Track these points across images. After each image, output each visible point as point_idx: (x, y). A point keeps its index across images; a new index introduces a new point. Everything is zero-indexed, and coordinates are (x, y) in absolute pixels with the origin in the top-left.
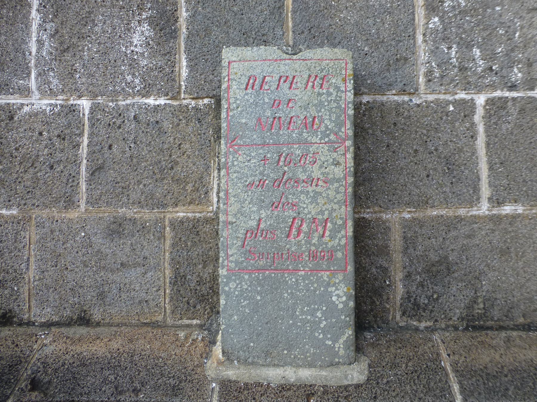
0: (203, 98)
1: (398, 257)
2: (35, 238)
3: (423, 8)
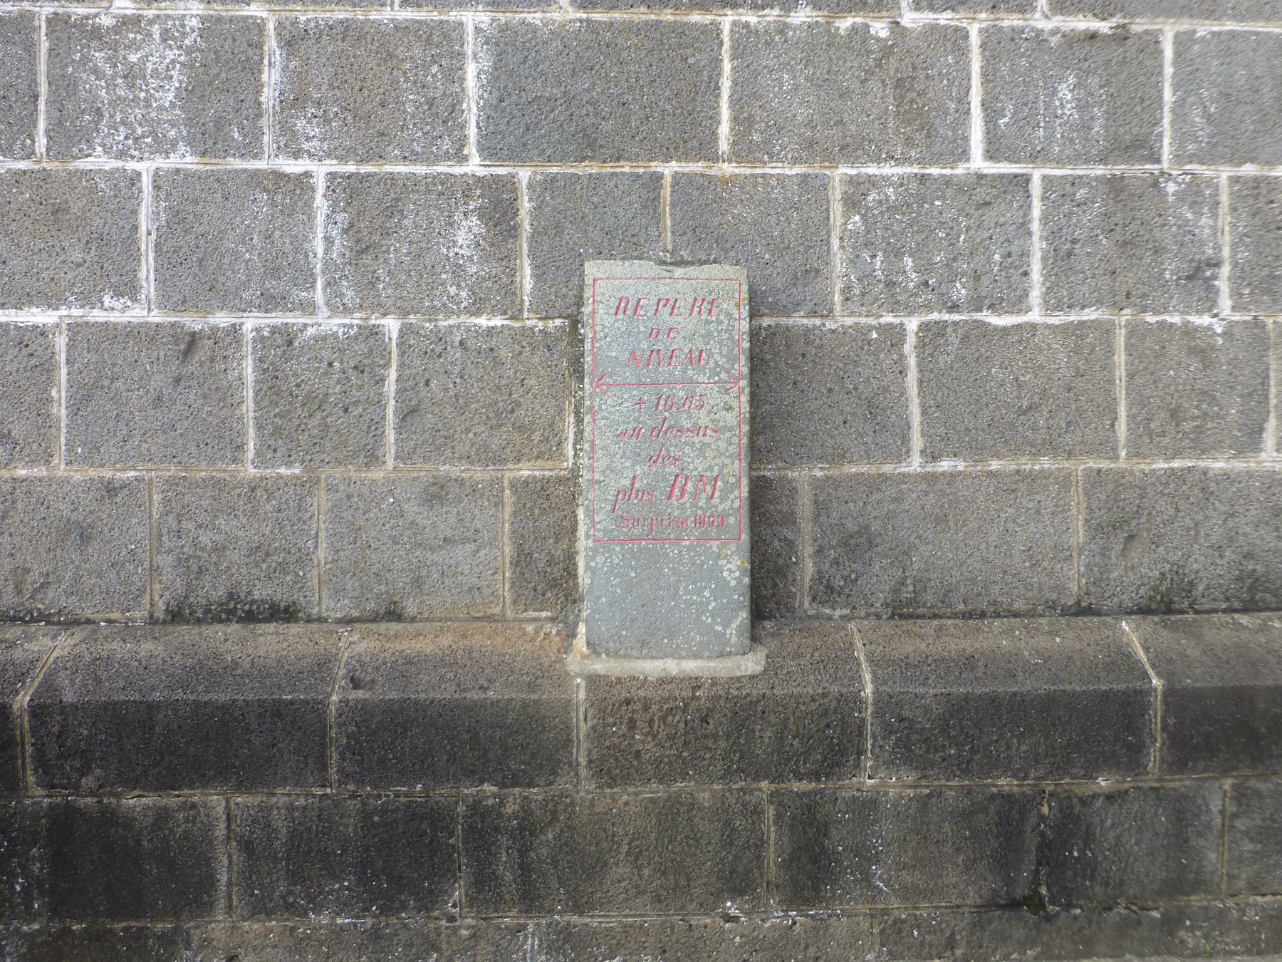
0: (553, 318)
1: (807, 527)
2: (325, 505)
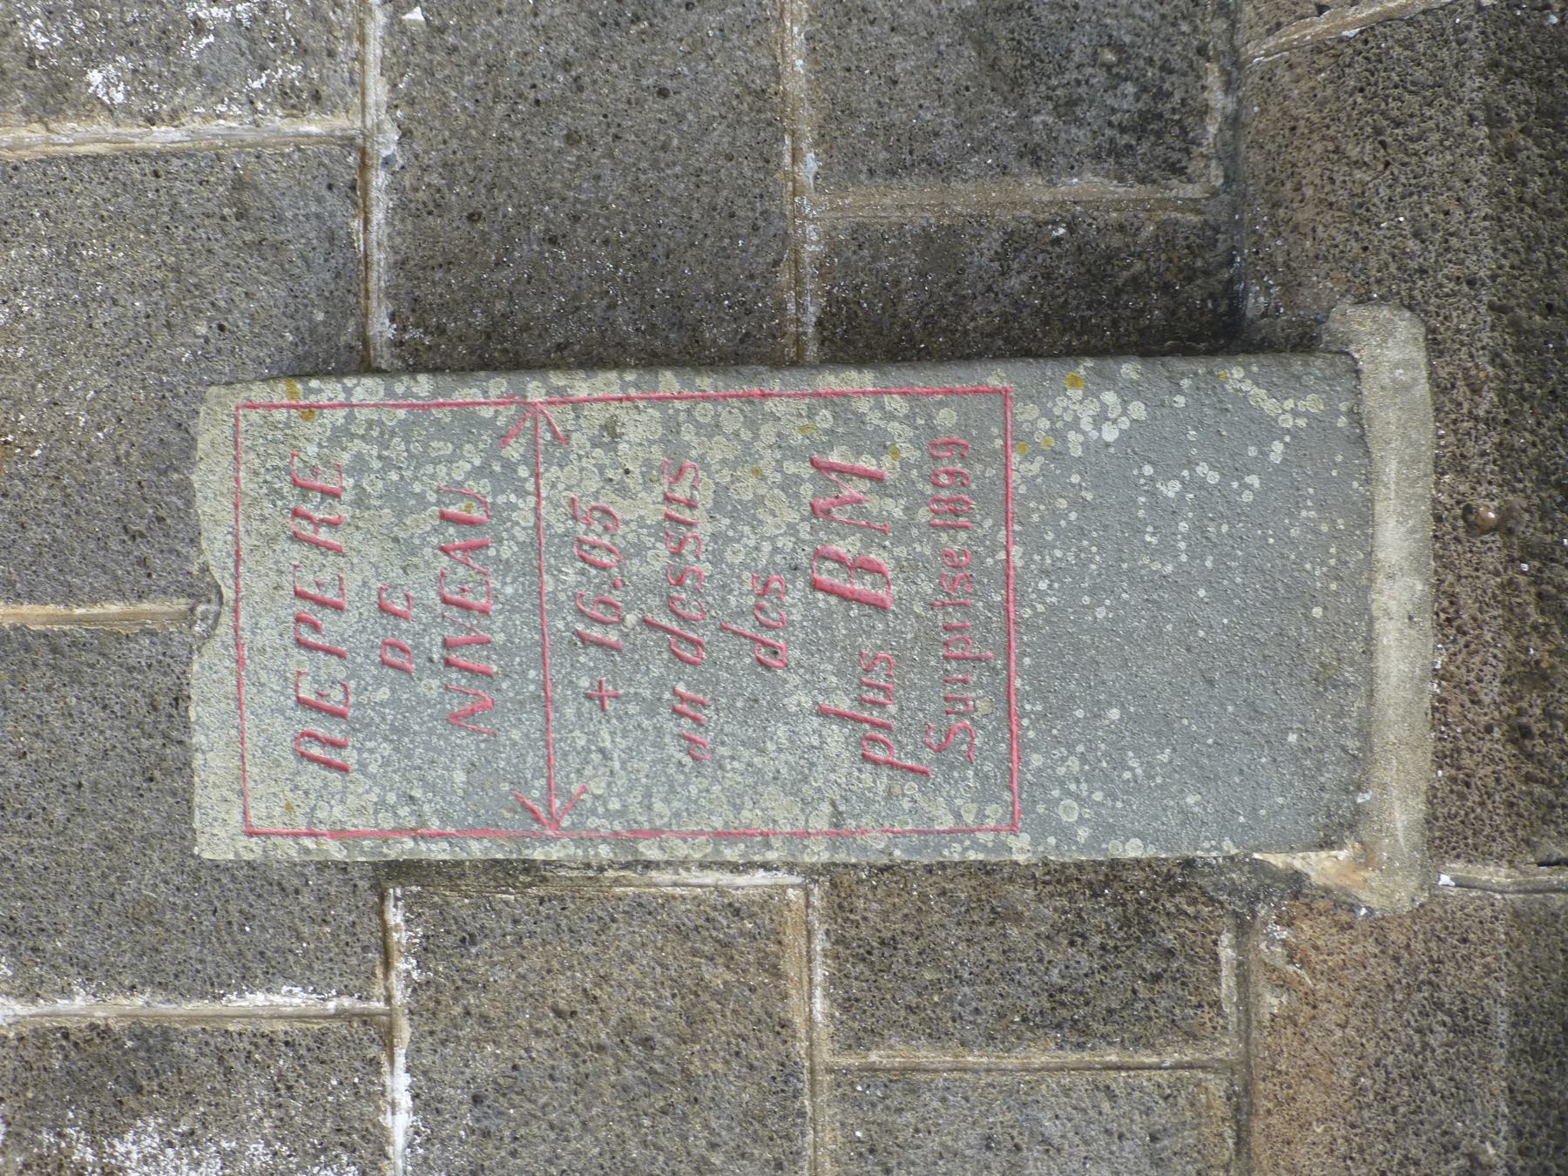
0: (385, 929)
1: (967, 196)
3: (53, 125)
